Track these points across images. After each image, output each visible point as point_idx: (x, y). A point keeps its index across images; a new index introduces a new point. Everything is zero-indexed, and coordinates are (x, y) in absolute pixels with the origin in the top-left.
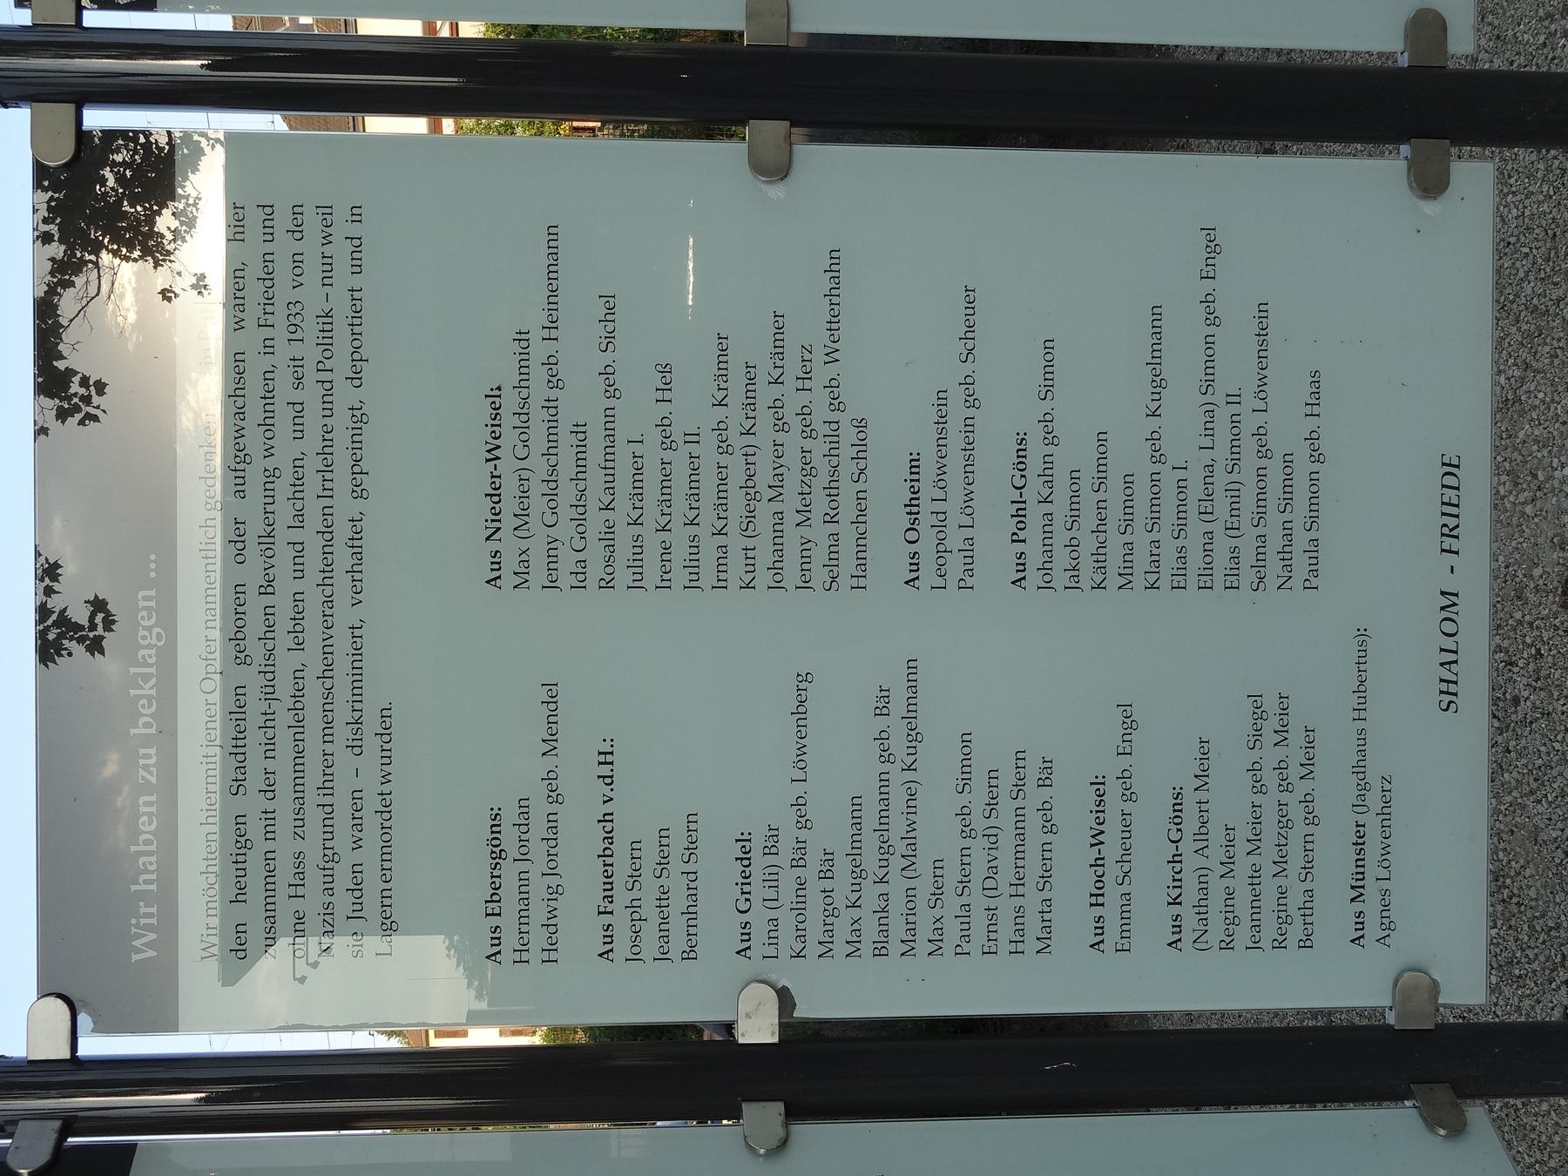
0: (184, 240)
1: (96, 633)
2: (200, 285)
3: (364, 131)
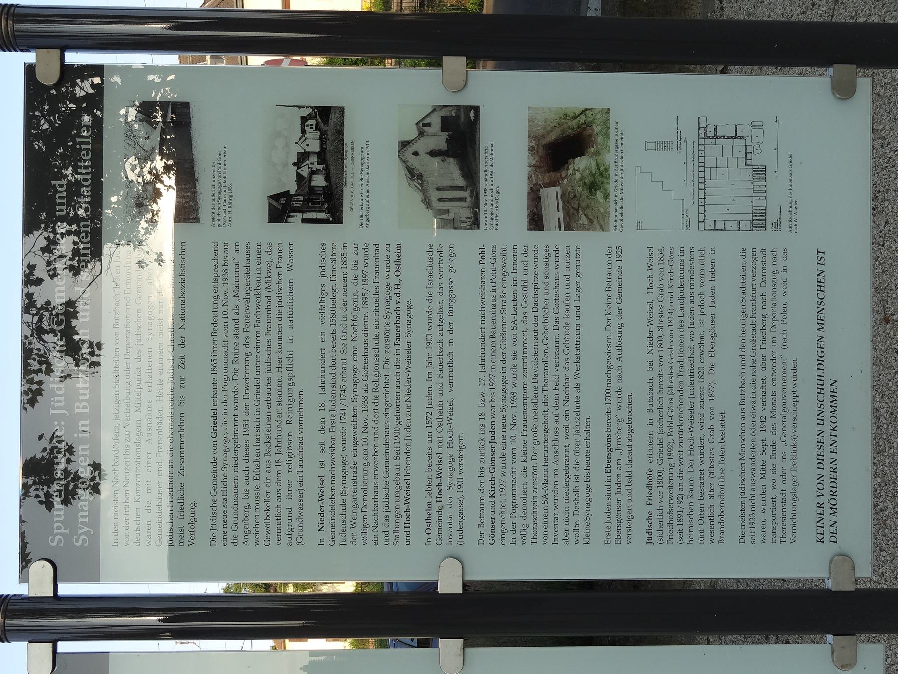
0: (150, 233)
1: (95, 482)
2: (160, 260)
3: (247, 64)
